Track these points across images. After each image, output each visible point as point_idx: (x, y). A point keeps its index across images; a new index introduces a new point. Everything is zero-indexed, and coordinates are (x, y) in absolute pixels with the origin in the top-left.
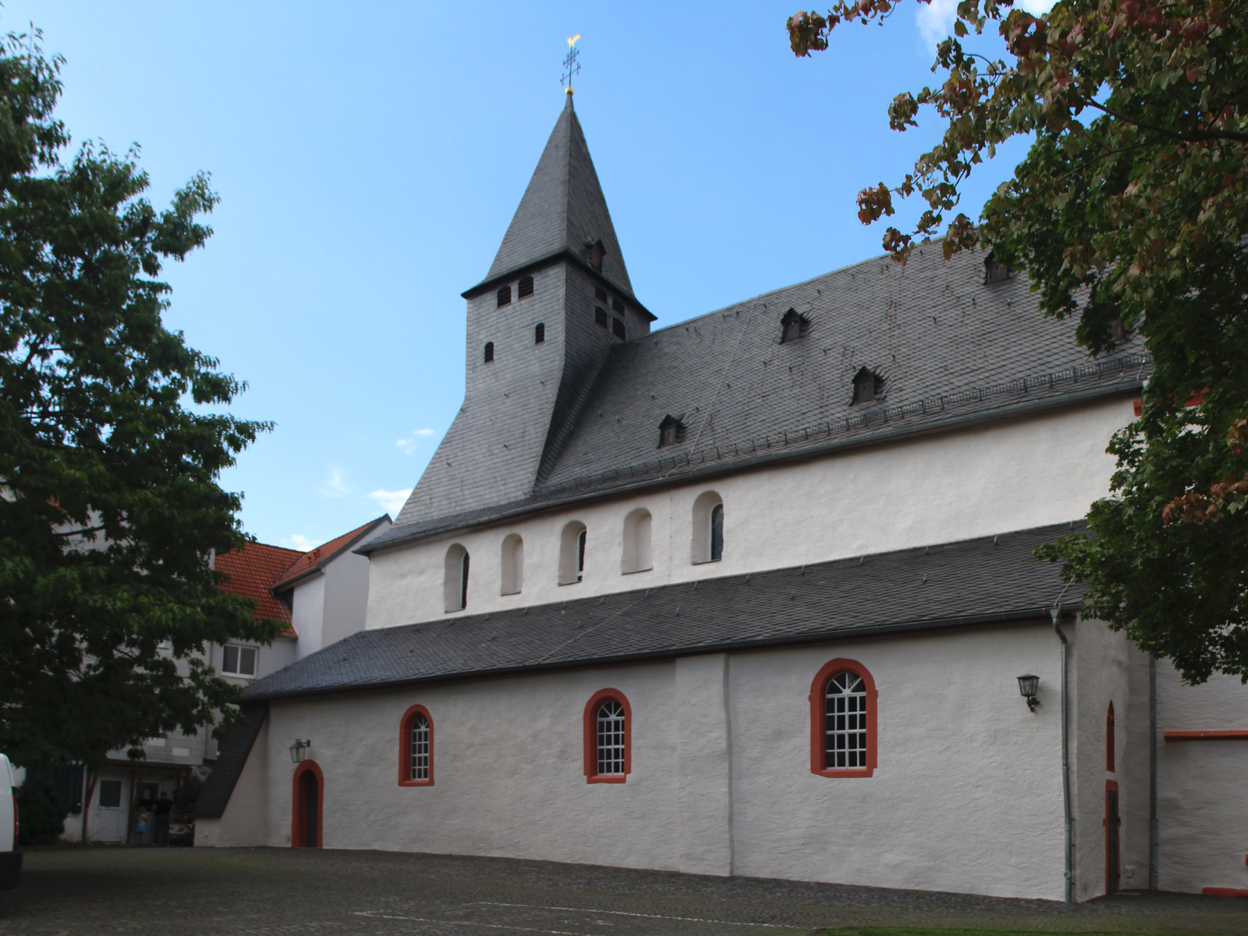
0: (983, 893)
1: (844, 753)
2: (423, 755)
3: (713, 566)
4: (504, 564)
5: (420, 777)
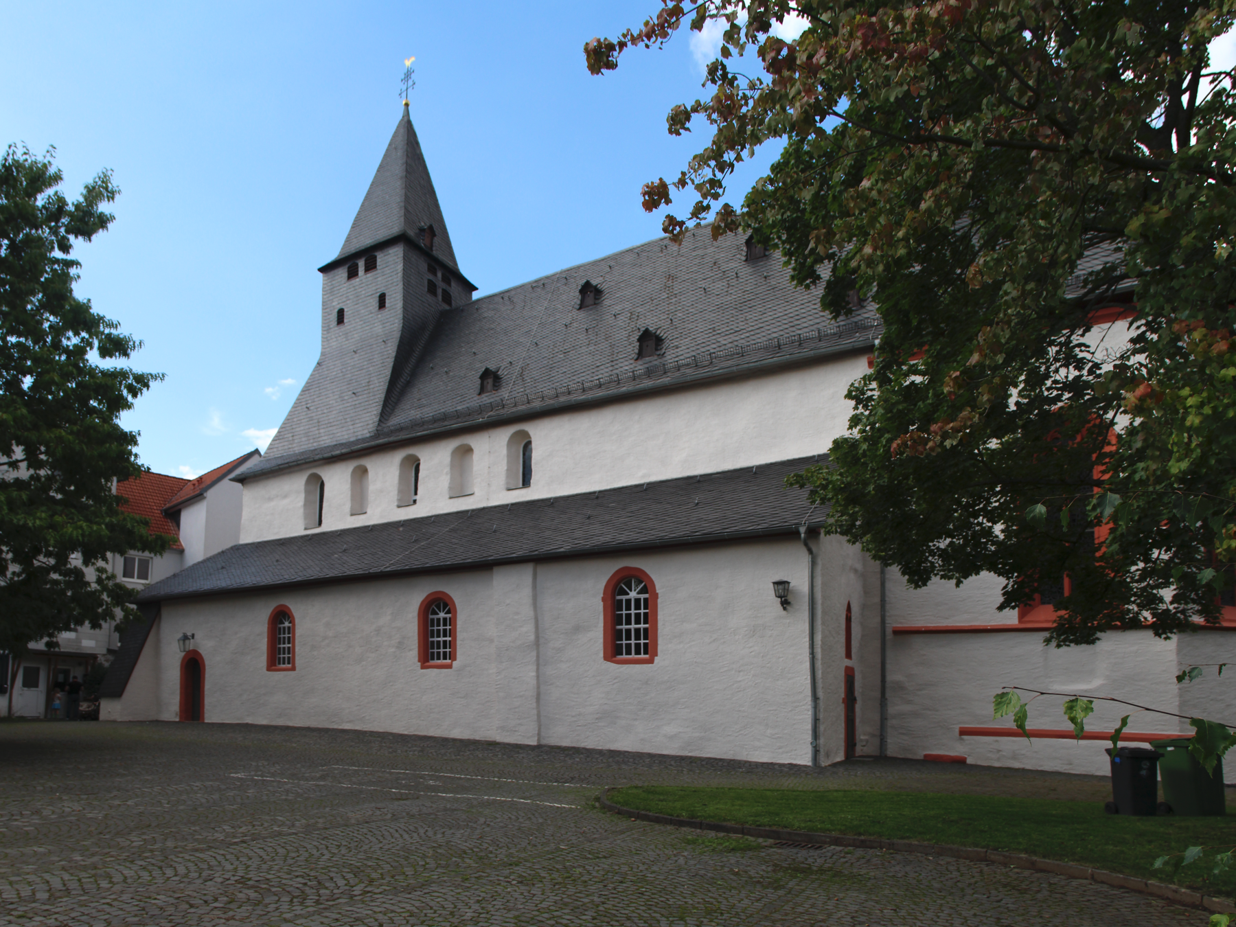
0: (745, 759)
3: (524, 491)
4: (353, 489)
5: (284, 663)
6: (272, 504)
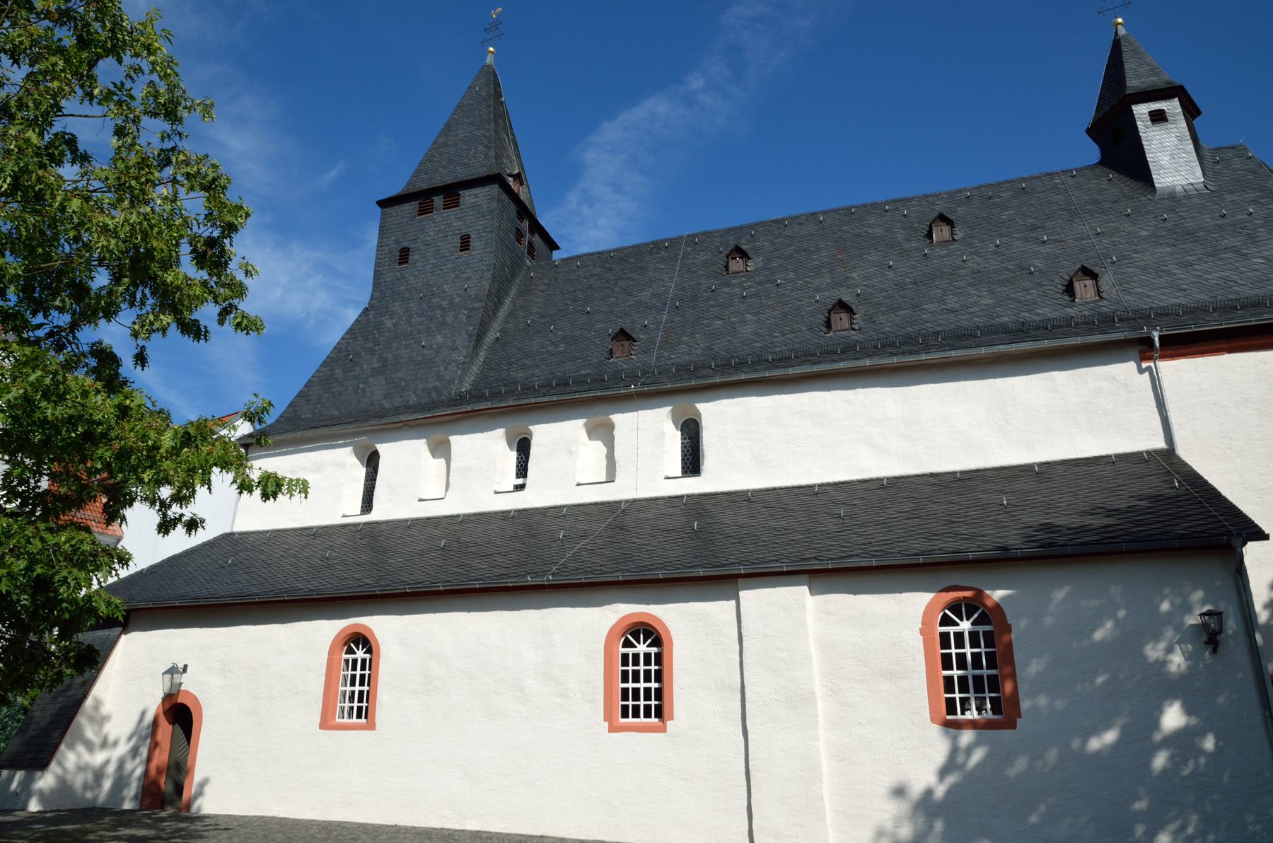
1: (645, 700)
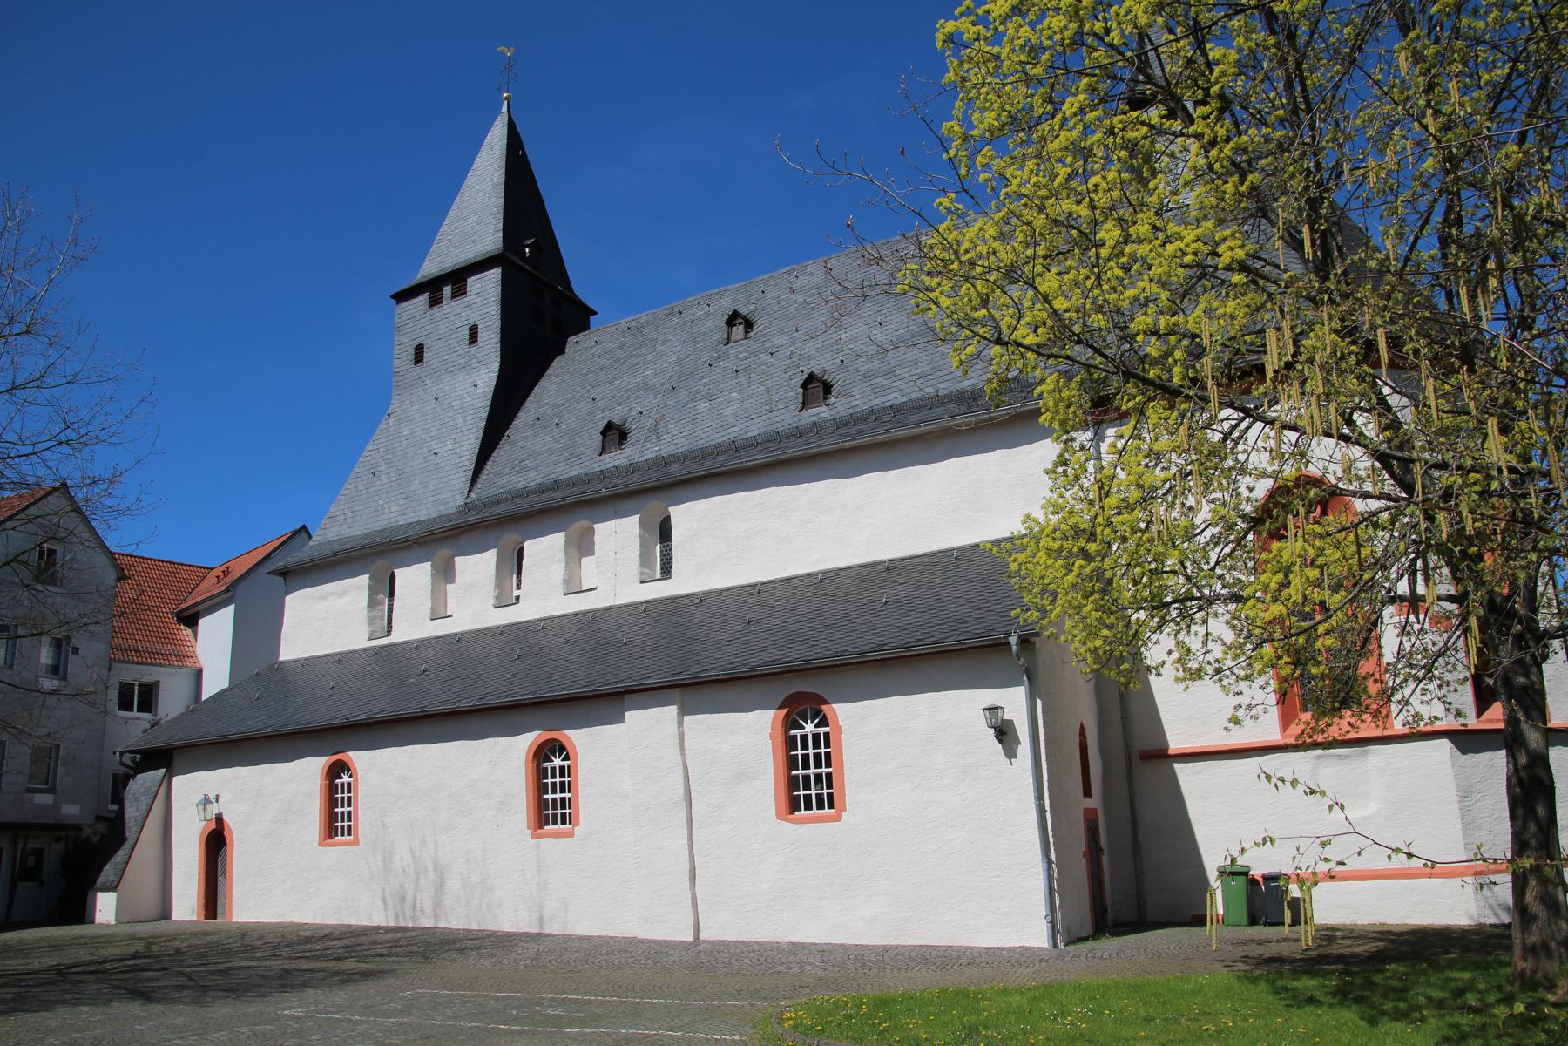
0: (966, 944)
2: (346, 809)
5: (342, 835)
6: (325, 604)
